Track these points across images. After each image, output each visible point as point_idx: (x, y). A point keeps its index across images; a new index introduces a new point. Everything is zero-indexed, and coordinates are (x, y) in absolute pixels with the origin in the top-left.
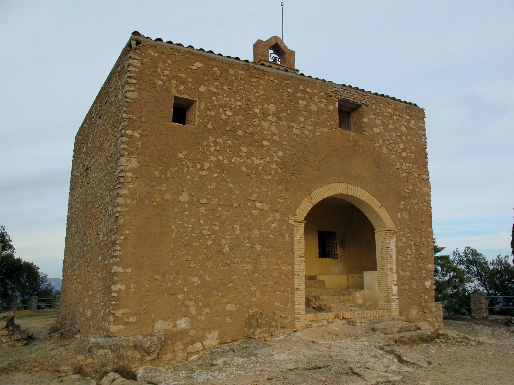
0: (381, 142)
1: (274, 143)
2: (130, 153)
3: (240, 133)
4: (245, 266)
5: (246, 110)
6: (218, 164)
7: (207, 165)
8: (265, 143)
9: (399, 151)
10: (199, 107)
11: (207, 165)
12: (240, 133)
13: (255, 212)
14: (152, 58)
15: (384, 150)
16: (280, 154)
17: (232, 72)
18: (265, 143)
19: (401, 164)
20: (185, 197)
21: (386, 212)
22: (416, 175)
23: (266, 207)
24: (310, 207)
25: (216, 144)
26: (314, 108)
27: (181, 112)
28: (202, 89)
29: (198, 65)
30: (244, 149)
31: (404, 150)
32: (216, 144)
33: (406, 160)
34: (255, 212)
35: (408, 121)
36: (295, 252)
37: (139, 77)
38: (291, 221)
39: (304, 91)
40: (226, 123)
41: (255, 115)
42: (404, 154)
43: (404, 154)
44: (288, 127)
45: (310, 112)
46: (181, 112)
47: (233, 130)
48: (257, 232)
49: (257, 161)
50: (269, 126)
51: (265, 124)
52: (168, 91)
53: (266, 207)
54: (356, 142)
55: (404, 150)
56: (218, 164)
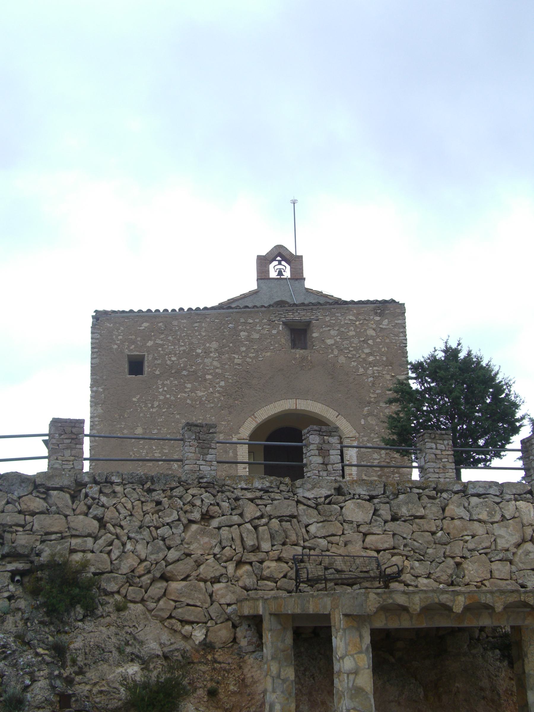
0: (336, 352)
1: (216, 375)
3: (185, 373)
7: (156, 404)
8: (208, 377)
9: (363, 356)
11: (156, 404)
12: (185, 373)
16: (222, 383)
18: (208, 377)
19: (366, 369)
26: (256, 336)
28: (150, 343)
29: (146, 325)
30: (189, 386)
31: (370, 354)
32: (163, 385)
33: (373, 364)
35: (379, 323)
39: (245, 323)
40: (171, 367)
41: (198, 355)
42: (371, 359)
43: (371, 359)
44: (230, 359)
45: (251, 341)
47: (178, 372)
49: (200, 394)
55: (370, 354)
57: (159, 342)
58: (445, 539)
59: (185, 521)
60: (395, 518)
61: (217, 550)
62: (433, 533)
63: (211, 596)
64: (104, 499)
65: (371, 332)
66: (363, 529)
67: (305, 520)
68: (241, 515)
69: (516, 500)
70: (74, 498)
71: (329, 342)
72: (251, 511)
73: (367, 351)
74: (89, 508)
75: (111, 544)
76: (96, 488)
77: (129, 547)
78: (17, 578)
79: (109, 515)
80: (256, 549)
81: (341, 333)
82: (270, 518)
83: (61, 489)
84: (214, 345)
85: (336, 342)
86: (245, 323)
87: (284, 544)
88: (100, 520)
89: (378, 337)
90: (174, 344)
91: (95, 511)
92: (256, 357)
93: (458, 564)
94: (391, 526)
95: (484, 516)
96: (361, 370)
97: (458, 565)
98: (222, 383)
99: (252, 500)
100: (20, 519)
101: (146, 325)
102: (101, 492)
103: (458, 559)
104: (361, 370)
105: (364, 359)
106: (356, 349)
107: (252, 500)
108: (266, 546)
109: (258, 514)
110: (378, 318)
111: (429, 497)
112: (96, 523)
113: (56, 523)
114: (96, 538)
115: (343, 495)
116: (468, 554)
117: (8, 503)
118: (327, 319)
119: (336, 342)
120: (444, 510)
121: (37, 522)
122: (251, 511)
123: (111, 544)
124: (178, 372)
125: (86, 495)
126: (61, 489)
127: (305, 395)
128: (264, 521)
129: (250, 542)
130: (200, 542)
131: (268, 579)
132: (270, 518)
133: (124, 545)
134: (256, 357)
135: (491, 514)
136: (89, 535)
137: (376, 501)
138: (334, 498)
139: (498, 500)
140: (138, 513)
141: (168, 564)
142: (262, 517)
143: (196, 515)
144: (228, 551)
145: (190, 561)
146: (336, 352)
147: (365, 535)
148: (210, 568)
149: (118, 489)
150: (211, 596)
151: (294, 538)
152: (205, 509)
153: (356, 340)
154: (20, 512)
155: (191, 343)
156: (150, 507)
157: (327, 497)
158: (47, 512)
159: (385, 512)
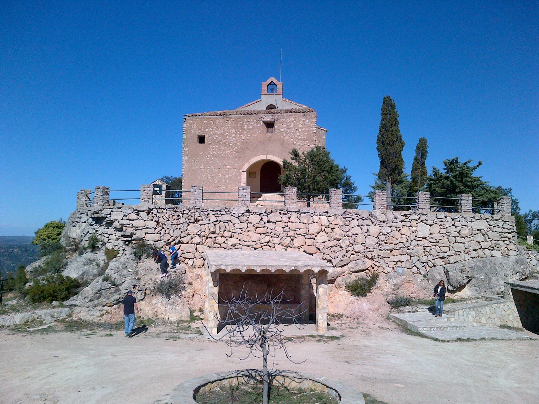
0: (284, 135)
1: (234, 144)
2: (185, 156)
3: (221, 143)
4: (223, 187)
5: (223, 134)
6: (213, 155)
7: (209, 156)
8: (231, 145)
9: (296, 136)
10: (206, 137)
11: (209, 156)
12: (221, 143)
13: (227, 169)
14: (190, 123)
15: (287, 138)
16: (236, 148)
17: (217, 121)
18: (231, 145)
19: (297, 142)
20: (202, 167)
21: (252, 160)
22: (306, 146)
23: (231, 167)
24: (248, 166)
25: (212, 148)
26: (251, 127)
27: (201, 139)
28: (207, 130)
29: (205, 121)
30: (223, 148)
31: (299, 135)
32: (212, 148)
33: (300, 140)
34: (227, 169)
35: (304, 121)
36: (434, 287)
37: (186, 131)
38: (241, 171)
39: (247, 121)
40: (216, 140)
41: (227, 135)
42: (300, 137)
43: (300, 137)
44: (240, 137)
45: (249, 129)
46: (201, 139)
47: (218, 142)
48: (227, 176)
49: (227, 152)
50: (232, 138)
51: (231, 138)
52: (195, 134)
53: (231, 167)
54: (270, 137)
55: (299, 135)
56: (213, 155)
57: (210, 129)
58: (288, 230)
59: (188, 222)
60: (268, 222)
61: (199, 233)
62: (283, 228)
63: (196, 249)
64: (158, 215)
65: (300, 126)
66: (256, 226)
67: (234, 222)
68: (209, 220)
69: (320, 215)
70: (148, 214)
71: (282, 130)
72: (213, 219)
73: (298, 134)
74: (153, 217)
75: (161, 230)
76: (156, 211)
77: (167, 232)
78: (127, 243)
79: (161, 220)
80: (214, 233)
81: (287, 126)
82: (220, 221)
83: (143, 211)
84: (234, 131)
85: (285, 130)
86: (247, 121)
87: (225, 231)
88: (158, 223)
89: (303, 128)
90: (217, 130)
91: (155, 219)
92: (251, 136)
93: (292, 240)
94: (267, 225)
95: (305, 221)
96: (295, 143)
97: (292, 240)
98: (236, 148)
99: (214, 214)
100: (128, 222)
101: (205, 121)
102: (158, 212)
103: (292, 238)
104: (295, 143)
105: (297, 138)
106: (293, 133)
107: (214, 214)
108: (218, 232)
109: (216, 220)
110: (304, 119)
111: (284, 214)
112: (156, 223)
113: (140, 223)
114: (155, 229)
115: (249, 213)
116: (296, 235)
117: (124, 216)
118: (282, 120)
119: (285, 130)
120: (289, 218)
121: (136, 223)
122: (213, 219)
123: (161, 230)
124: (218, 142)
125: (152, 213)
126: (143, 211)
127: (271, 153)
128: (218, 222)
129: (212, 230)
130: (193, 229)
131: (217, 244)
132: (220, 221)
133: (166, 231)
134: (251, 136)
135: (308, 221)
136: (153, 228)
137: (262, 215)
138: (245, 214)
139: (312, 215)
140: (171, 219)
141: (181, 238)
142: (217, 221)
143: (192, 220)
144: (203, 234)
145: (189, 237)
146: (284, 135)
147: (256, 228)
148: (197, 240)
149: (165, 211)
150: (196, 249)
151: (228, 229)
152: (196, 218)
153: (293, 129)
154: (128, 219)
155: (224, 130)
156: (175, 217)
157: (243, 214)
158: (138, 219)
159: (265, 219)
